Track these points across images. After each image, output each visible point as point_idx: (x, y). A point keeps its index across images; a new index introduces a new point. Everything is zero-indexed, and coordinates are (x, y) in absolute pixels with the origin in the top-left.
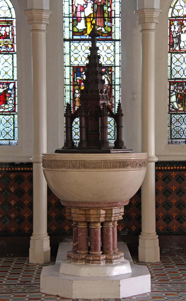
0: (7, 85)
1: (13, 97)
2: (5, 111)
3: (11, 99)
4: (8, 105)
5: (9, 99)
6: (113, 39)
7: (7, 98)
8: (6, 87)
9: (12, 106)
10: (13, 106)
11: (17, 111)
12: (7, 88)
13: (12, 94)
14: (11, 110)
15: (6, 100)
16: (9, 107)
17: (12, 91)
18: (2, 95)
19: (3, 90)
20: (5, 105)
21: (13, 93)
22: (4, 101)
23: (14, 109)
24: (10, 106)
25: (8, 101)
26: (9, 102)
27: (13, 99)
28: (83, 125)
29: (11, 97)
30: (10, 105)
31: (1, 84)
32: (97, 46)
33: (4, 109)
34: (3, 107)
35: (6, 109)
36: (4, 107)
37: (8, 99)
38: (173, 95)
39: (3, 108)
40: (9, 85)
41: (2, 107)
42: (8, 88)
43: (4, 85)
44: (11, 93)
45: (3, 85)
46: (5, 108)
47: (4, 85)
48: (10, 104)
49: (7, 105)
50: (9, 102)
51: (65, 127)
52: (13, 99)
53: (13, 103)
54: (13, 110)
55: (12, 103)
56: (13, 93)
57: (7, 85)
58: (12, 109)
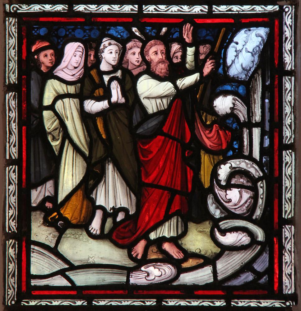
0: (204, 49)
1: (256, 154)
2: (187, 278)
3: (245, 173)
4: (215, 223)
5: (224, 171)
6: (176, 142)
7: (206, 160)
8: (199, 66)
9: (245, 239)
10: (260, 234)
11: (288, 286)
12: (208, 68)
13: (250, 125)
14: (236, 275)
15: (197, 180)
16: (225, 249)
17: (247, 100)
18: (158, 131)
19: (167, 87)
20: (184, 233)
21: (257, 118)
22: (173, 192)
23: (260, 266)
24: (229, 239)
25: (211, 190)
26: (217, 200)
27: (255, 171)
28: (276, 201)
29: (239, 155)
30: (223, 225)
31: (158, 37)
32: (46, 206)
33: (177, 264)
34: (167, 246)
35: (191, 263)
36: (175, 241)
37: (214, 175)
38: (210, 157)
39: (167, 259)
40: (225, 47)
41: (163, 239)
42: (213, 72)
43: (184, 46)
44: (242, 116)
45: (167, 41)
46: (188, 255)
47: (184, 46)
48: (230, 215)
49: (207, 226)
50: (217, 200)
51: (10, 88)
52: (255, 171)
53: (258, 212)
54: (259, 275)
55: (252, 209)
56: (257, 118)
57: (204, 49)
58: (247, 267)
